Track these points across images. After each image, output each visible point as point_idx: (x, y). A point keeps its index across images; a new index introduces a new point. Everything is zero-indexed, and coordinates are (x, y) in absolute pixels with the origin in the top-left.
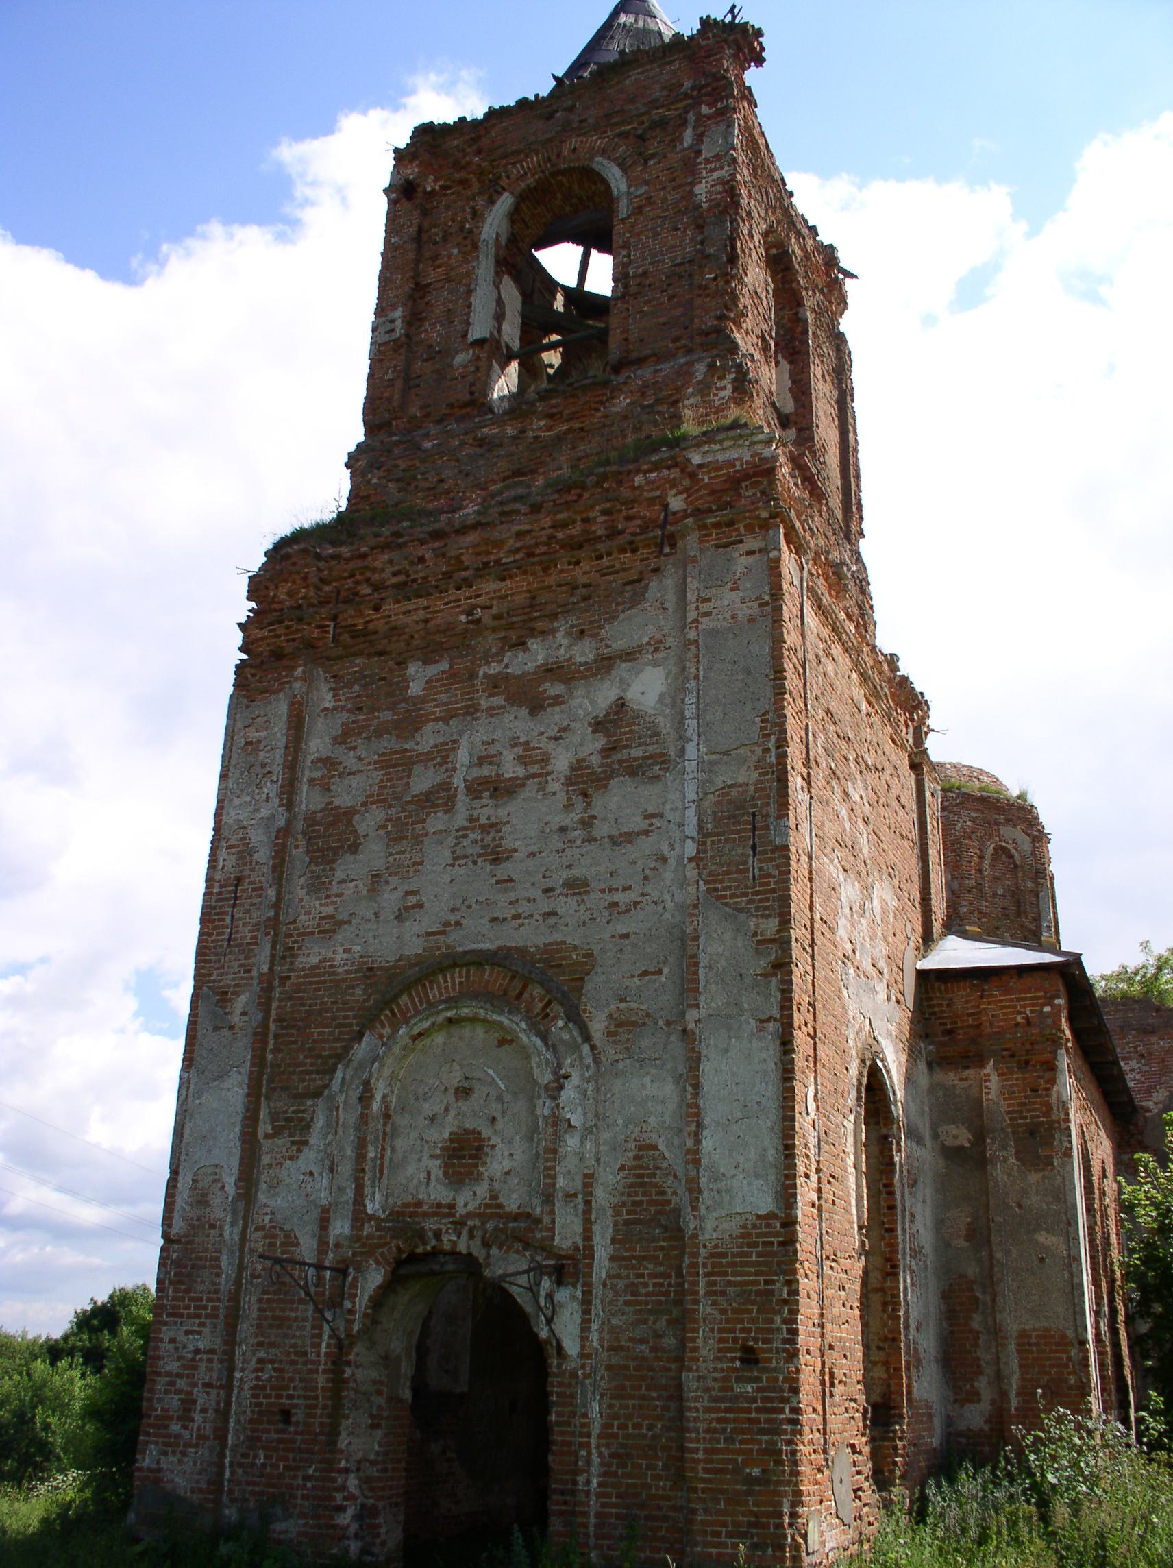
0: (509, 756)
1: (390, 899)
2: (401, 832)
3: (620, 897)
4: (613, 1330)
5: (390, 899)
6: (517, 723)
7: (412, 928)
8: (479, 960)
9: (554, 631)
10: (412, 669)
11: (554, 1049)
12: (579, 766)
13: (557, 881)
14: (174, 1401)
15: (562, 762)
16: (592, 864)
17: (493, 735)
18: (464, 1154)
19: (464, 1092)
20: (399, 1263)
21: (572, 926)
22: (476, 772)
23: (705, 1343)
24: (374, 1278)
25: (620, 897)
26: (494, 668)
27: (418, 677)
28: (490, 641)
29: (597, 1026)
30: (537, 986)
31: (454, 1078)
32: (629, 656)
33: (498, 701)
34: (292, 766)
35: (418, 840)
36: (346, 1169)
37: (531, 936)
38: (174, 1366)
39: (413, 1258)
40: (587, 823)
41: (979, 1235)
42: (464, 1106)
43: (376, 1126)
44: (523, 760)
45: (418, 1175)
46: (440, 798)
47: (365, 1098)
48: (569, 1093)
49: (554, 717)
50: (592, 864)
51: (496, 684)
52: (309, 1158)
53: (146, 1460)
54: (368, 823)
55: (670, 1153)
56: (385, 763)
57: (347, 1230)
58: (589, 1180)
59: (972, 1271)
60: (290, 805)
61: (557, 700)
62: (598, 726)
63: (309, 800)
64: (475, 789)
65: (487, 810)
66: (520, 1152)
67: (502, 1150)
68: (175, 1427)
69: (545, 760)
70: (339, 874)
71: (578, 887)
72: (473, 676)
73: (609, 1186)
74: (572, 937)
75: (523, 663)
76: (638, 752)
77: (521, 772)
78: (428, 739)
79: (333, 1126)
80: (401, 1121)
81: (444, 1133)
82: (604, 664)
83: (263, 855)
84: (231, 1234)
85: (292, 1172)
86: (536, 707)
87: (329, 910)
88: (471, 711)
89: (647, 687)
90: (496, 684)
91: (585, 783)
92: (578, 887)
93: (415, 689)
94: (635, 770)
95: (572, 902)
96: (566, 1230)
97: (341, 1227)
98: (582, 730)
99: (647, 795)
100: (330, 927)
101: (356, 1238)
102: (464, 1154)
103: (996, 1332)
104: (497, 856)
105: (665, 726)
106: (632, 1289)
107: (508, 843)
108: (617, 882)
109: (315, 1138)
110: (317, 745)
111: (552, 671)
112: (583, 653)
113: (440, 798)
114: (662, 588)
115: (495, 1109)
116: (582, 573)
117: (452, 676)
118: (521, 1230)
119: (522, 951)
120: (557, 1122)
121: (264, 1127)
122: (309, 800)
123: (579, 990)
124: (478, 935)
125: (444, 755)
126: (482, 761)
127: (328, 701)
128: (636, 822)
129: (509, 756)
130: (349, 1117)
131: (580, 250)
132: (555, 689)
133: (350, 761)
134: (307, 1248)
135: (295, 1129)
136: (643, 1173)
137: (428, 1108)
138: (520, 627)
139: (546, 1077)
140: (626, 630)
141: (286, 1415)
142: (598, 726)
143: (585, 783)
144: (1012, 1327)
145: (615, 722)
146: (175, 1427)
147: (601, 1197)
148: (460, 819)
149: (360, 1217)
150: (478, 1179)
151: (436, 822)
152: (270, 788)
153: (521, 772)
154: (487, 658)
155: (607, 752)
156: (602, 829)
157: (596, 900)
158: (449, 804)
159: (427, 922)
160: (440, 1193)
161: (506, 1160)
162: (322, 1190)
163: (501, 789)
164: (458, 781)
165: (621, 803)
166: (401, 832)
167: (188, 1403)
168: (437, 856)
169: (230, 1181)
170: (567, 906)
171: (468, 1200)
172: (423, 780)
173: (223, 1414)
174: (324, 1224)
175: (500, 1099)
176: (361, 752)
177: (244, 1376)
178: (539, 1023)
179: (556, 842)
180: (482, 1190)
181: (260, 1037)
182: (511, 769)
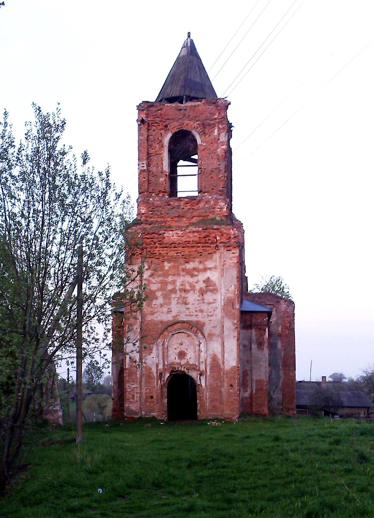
0: (187, 285)
3: (209, 313)
4: (210, 383)
5: (165, 309)
6: (188, 278)
8: (183, 322)
9: (195, 261)
10: (166, 263)
11: (198, 338)
12: (201, 288)
13: (198, 309)
14: (131, 396)
18: (182, 355)
19: (181, 344)
20: (171, 372)
21: (201, 318)
22: (181, 287)
23: (226, 384)
25: (209, 313)
26: (184, 267)
27: (167, 265)
30: (195, 328)
31: (179, 342)
32: (210, 269)
33: (184, 273)
37: (193, 319)
38: (130, 390)
40: (203, 300)
42: (181, 346)
45: (173, 357)
46: (174, 291)
50: (204, 307)
51: (183, 270)
52: (152, 355)
53: (127, 405)
55: (219, 356)
56: (161, 282)
57: (162, 367)
58: (206, 360)
61: (196, 275)
62: (204, 282)
64: (181, 290)
65: (183, 294)
67: (189, 354)
68: (131, 400)
70: (154, 303)
72: (178, 267)
73: (209, 360)
76: (212, 288)
77: (190, 288)
78: (170, 279)
79: (157, 349)
82: (205, 270)
86: (192, 276)
87: (152, 310)
89: (214, 276)
90: (183, 270)
91: (202, 292)
92: (202, 311)
93: (166, 268)
94: (211, 291)
95: (201, 313)
96: (202, 367)
97: (161, 367)
99: (214, 297)
100: (152, 313)
101: (164, 368)
102: (182, 355)
103: (252, 379)
104: (186, 303)
105: (217, 284)
106: (213, 376)
107: (188, 301)
108: (210, 311)
111: (194, 269)
112: (201, 267)
113: (174, 291)
114: (216, 256)
115: (187, 347)
116: (200, 250)
117: (174, 267)
118: (194, 368)
119: (192, 321)
123: (203, 329)
125: (174, 282)
126: (182, 285)
128: (212, 301)
131: (178, 177)
132: (196, 273)
133: (153, 281)
134: (154, 370)
136: (214, 359)
137: (175, 347)
139: (198, 343)
140: (209, 264)
141: (152, 397)
142: (204, 282)
143: (202, 292)
144: (254, 378)
145: (208, 281)
146: (131, 400)
147: (208, 363)
148: (178, 296)
149: (164, 365)
150: (185, 359)
151: (173, 296)
153: (190, 288)
154: (181, 264)
155: (207, 286)
156: (206, 301)
157: (205, 314)
159: (174, 313)
160: (178, 361)
162: (156, 360)
164: (177, 288)
165: (209, 297)
166: (167, 296)
167: (133, 396)
168: (174, 302)
170: (200, 314)
171: (183, 362)
172: (170, 287)
175: (188, 345)
176: (156, 279)
177: (144, 391)
178: (196, 334)
179: (197, 302)
180: (186, 361)
182: (188, 287)
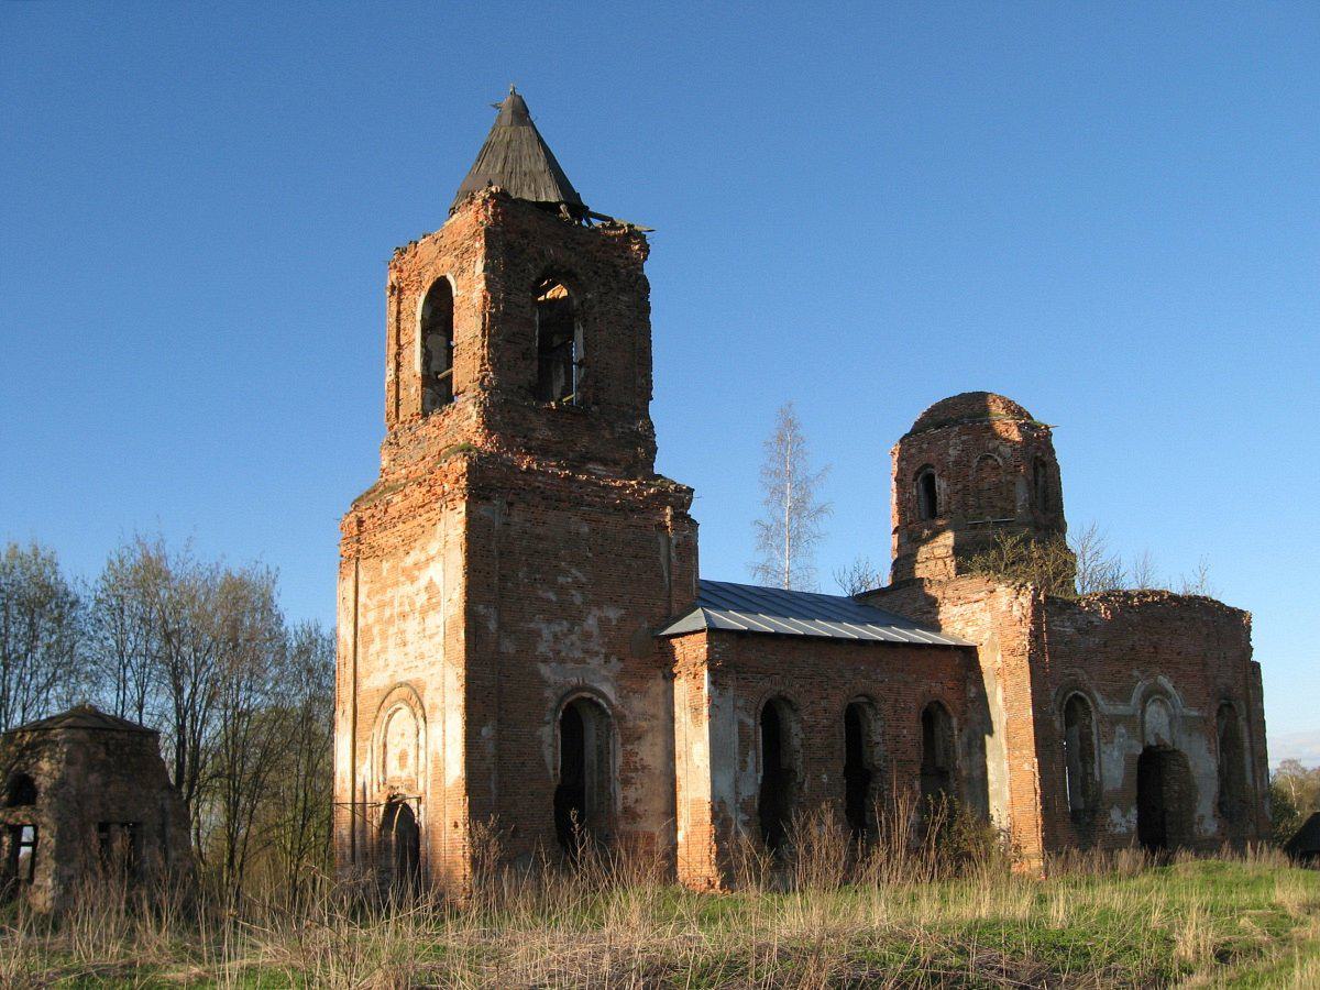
1: (381, 662)
5: (381, 662)
15: (418, 605)
35: (387, 638)
40: (424, 630)
46: (390, 621)
49: (416, 585)
75: (409, 561)
82: (430, 559)
86: (413, 580)
143: (424, 612)
156: (427, 633)
172: (388, 613)
182: (407, 609)
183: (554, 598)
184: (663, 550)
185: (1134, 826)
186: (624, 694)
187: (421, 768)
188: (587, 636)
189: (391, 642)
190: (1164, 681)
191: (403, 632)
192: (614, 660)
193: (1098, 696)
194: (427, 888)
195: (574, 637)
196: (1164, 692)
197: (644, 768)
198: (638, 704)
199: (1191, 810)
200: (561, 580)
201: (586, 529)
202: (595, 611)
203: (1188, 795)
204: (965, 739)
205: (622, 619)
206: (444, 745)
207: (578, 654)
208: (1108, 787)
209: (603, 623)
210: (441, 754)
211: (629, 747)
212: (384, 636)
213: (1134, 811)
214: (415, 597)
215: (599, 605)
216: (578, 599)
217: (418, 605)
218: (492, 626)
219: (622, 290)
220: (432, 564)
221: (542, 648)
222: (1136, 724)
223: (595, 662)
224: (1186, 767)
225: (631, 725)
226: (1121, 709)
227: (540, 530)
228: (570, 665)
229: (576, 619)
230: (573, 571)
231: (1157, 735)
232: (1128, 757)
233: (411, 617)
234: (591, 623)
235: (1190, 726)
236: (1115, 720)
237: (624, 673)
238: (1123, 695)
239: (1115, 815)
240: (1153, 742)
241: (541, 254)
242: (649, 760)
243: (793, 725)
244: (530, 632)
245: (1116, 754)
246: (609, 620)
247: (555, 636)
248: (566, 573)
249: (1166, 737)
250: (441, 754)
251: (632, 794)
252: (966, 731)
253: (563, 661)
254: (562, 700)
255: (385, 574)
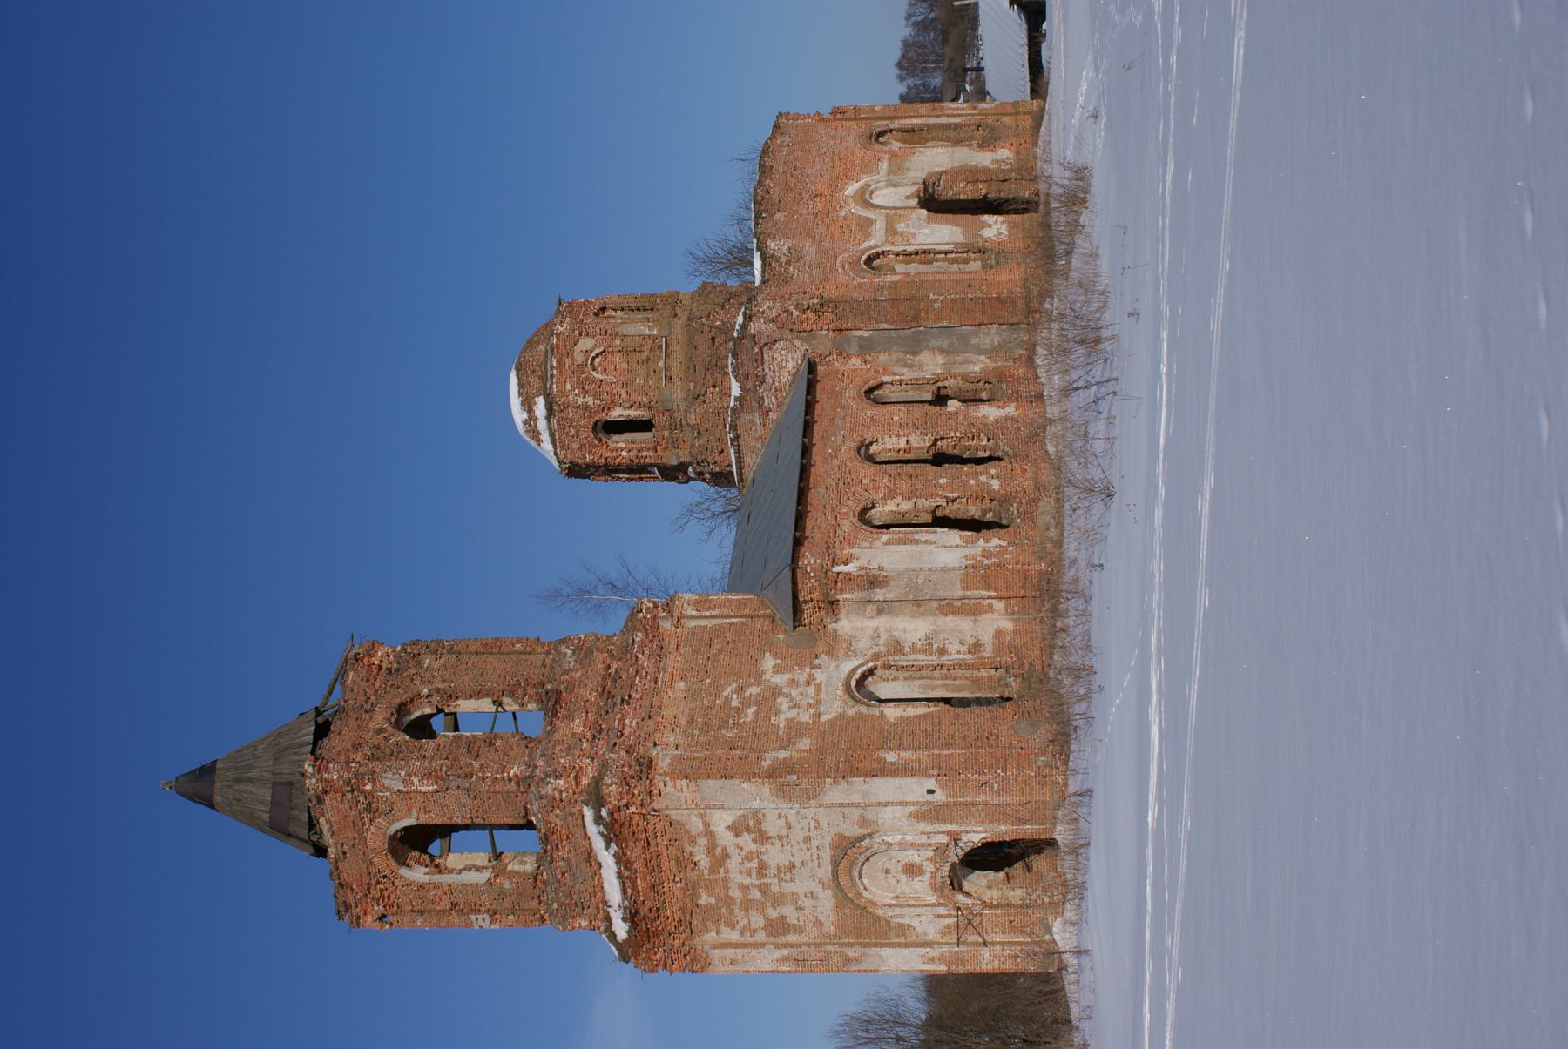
0: (748, 865)
1: (808, 903)
2: (779, 900)
5: (808, 903)
7: (821, 895)
8: (835, 872)
10: (701, 902)
12: (755, 841)
15: (753, 847)
16: (798, 835)
17: (735, 870)
18: (912, 870)
19: (887, 871)
23: (981, 798)
24: (960, 898)
27: (705, 899)
28: (692, 875)
29: (863, 831)
33: (722, 870)
34: (744, 945)
35: (782, 895)
36: (918, 910)
37: (827, 855)
39: (952, 884)
40: (781, 838)
41: (918, 603)
43: (902, 902)
44: (750, 860)
45: (920, 887)
46: (764, 889)
47: (891, 906)
48: (890, 839)
49: (732, 850)
52: (915, 923)
54: (773, 913)
55: (912, 809)
59: (935, 604)
60: (762, 945)
63: (761, 937)
66: (909, 852)
69: (751, 853)
71: (808, 839)
73: (924, 826)
74: (828, 840)
75: (703, 861)
78: (737, 894)
79: (902, 916)
80: (899, 891)
81: (903, 877)
82: (709, 833)
83: (785, 952)
84: (945, 948)
85: (920, 929)
86: (726, 856)
88: (725, 880)
92: (808, 839)
97: (942, 911)
98: (740, 840)
102: (912, 870)
104: (792, 866)
109: (906, 921)
110: (734, 936)
111: (710, 850)
113: (764, 889)
118: (941, 851)
120: (900, 844)
121: (902, 939)
122: (761, 937)
124: (826, 871)
125: (744, 888)
127: (713, 934)
128: (782, 822)
129: (748, 865)
130: (898, 911)
135: (903, 929)
136: (920, 816)
138: (686, 863)
140: (696, 825)
142: (737, 835)
143: (762, 838)
144: (959, 593)
145: (736, 829)
149: (939, 905)
151: (775, 889)
152: (754, 952)
155: (749, 831)
156: (784, 833)
158: (767, 885)
159: (818, 889)
160: (927, 877)
161: (914, 857)
163: (762, 867)
165: (772, 826)
169: (924, 951)
170: (815, 843)
171: (929, 868)
172: (756, 895)
173: (1013, 943)
174: (940, 916)
181: (866, 945)
182: (754, 864)
183: (754, 709)
184: (703, 623)
185: (1000, 218)
186: (851, 653)
187: (924, 839)
188: (793, 683)
189: (789, 888)
190: (851, 189)
191: (779, 869)
192: (817, 662)
193: (867, 244)
194: (905, 141)
195: (794, 693)
196: (863, 191)
197: (928, 638)
198: (863, 643)
199: (986, 170)
200: (734, 703)
201: (682, 685)
202: (767, 676)
203: (971, 174)
204: (905, 370)
205: (776, 656)
206: (901, 803)
207: (811, 690)
208: (960, 238)
209: (778, 670)
210: (912, 809)
211: (907, 650)
212: (779, 900)
213: (986, 218)
214: (746, 850)
215: (760, 674)
216: (754, 690)
217: (753, 847)
218: (783, 755)
219: (418, 664)
220: (713, 828)
221: (805, 717)
222: (893, 216)
223: (819, 676)
224: (941, 174)
225: (883, 649)
226: (880, 225)
227: (683, 721)
228: (823, 696)
229: (776, 691)
230: (725, 693)
231: (907, 198)
232: (929, 221)
233: (764, 858)
234: (780, 680)
235: (897, 167)
236: (891, 231)
237: (831, 653)
238: (865, 225)
239: (988, 233)
240: (916, 201)
241: (379, 731)
242: (921, 634)
243: (887, 508)
244: (788, 727)
245: (927, 231)
246: (775, 666)
247: (791, 708)
248: (728, 700)
249: (911, 190)
250: (912, 809)
251: (954, 647)
252: (896, 369)
253: (819, 702)
254: (857, 701)
255: (713, 901)
